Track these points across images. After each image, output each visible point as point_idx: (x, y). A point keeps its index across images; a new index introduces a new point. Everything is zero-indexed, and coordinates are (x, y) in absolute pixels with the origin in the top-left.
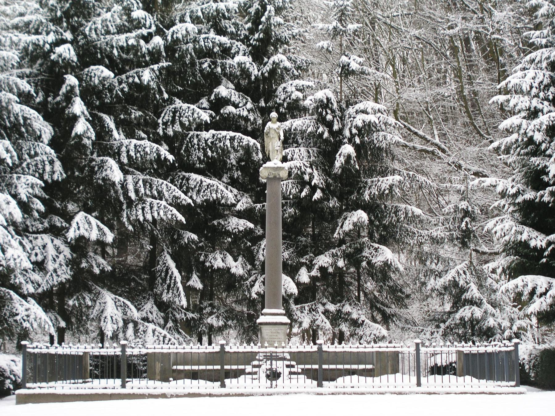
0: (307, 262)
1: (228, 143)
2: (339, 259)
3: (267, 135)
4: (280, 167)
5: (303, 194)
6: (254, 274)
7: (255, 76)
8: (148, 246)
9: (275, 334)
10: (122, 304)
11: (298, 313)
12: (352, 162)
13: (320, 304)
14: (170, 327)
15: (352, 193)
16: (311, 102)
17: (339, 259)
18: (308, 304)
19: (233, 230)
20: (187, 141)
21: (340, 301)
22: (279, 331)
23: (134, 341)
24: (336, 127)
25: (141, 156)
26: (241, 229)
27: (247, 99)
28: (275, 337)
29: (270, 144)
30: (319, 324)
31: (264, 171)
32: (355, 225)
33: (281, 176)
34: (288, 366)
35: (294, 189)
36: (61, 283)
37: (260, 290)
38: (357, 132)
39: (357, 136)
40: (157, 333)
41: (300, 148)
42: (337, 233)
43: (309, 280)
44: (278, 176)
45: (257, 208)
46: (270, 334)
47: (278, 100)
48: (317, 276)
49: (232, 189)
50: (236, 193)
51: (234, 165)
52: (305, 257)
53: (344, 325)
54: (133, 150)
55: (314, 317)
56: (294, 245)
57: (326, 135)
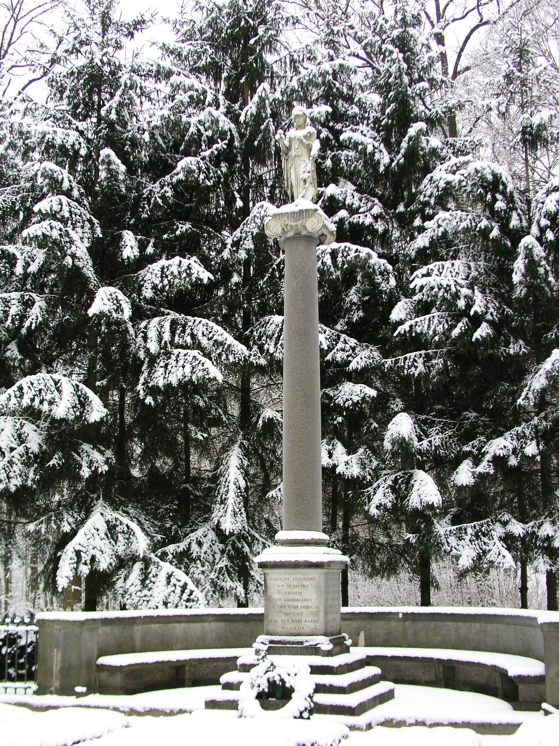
0: (474, 450)
1: (328, 260)
2: (528, 442)
4: (307, 211)
5: (456, 332)
6: (385, 475)
7: (384, 165)
8: (199, 433)
9: (296, 590)
10: (126, 529)
11: (453, 540)
12: (541, 270)
13: (498, 524)
14: (221, 569)
15: (550, 329)
16: (462, 178)
17: (528, 442)
18: (472, 524)
19: (344, 404)
20: (274, 269)
21: (535, 517)
22: (306, 583)
23: (139, 593)
24: (514, 222)
25: (169, 282)
26: (356, 399)
27: (373, 202)
28: (297, 597)
30: (492, 558)
31: (273, 223)
33: (310, 229)
34: (316, 670)
35: (441, 326)
37: (384, 501)
38: (548, 223)
39: (548, 230)
40: (173, 580)
41: (453, 261)
42: (523, 396)
43: (473, 480)
44: (304, 233)
45: (386, 366)
48: (488, 473)
49: (347, 338)
50: (353, 345)
51: (354, 304)
52: (471, 443)
53: (541, 560)
54: (159, 275)
55: (484, 547)
56: (455, 425)
57: (495, 233)
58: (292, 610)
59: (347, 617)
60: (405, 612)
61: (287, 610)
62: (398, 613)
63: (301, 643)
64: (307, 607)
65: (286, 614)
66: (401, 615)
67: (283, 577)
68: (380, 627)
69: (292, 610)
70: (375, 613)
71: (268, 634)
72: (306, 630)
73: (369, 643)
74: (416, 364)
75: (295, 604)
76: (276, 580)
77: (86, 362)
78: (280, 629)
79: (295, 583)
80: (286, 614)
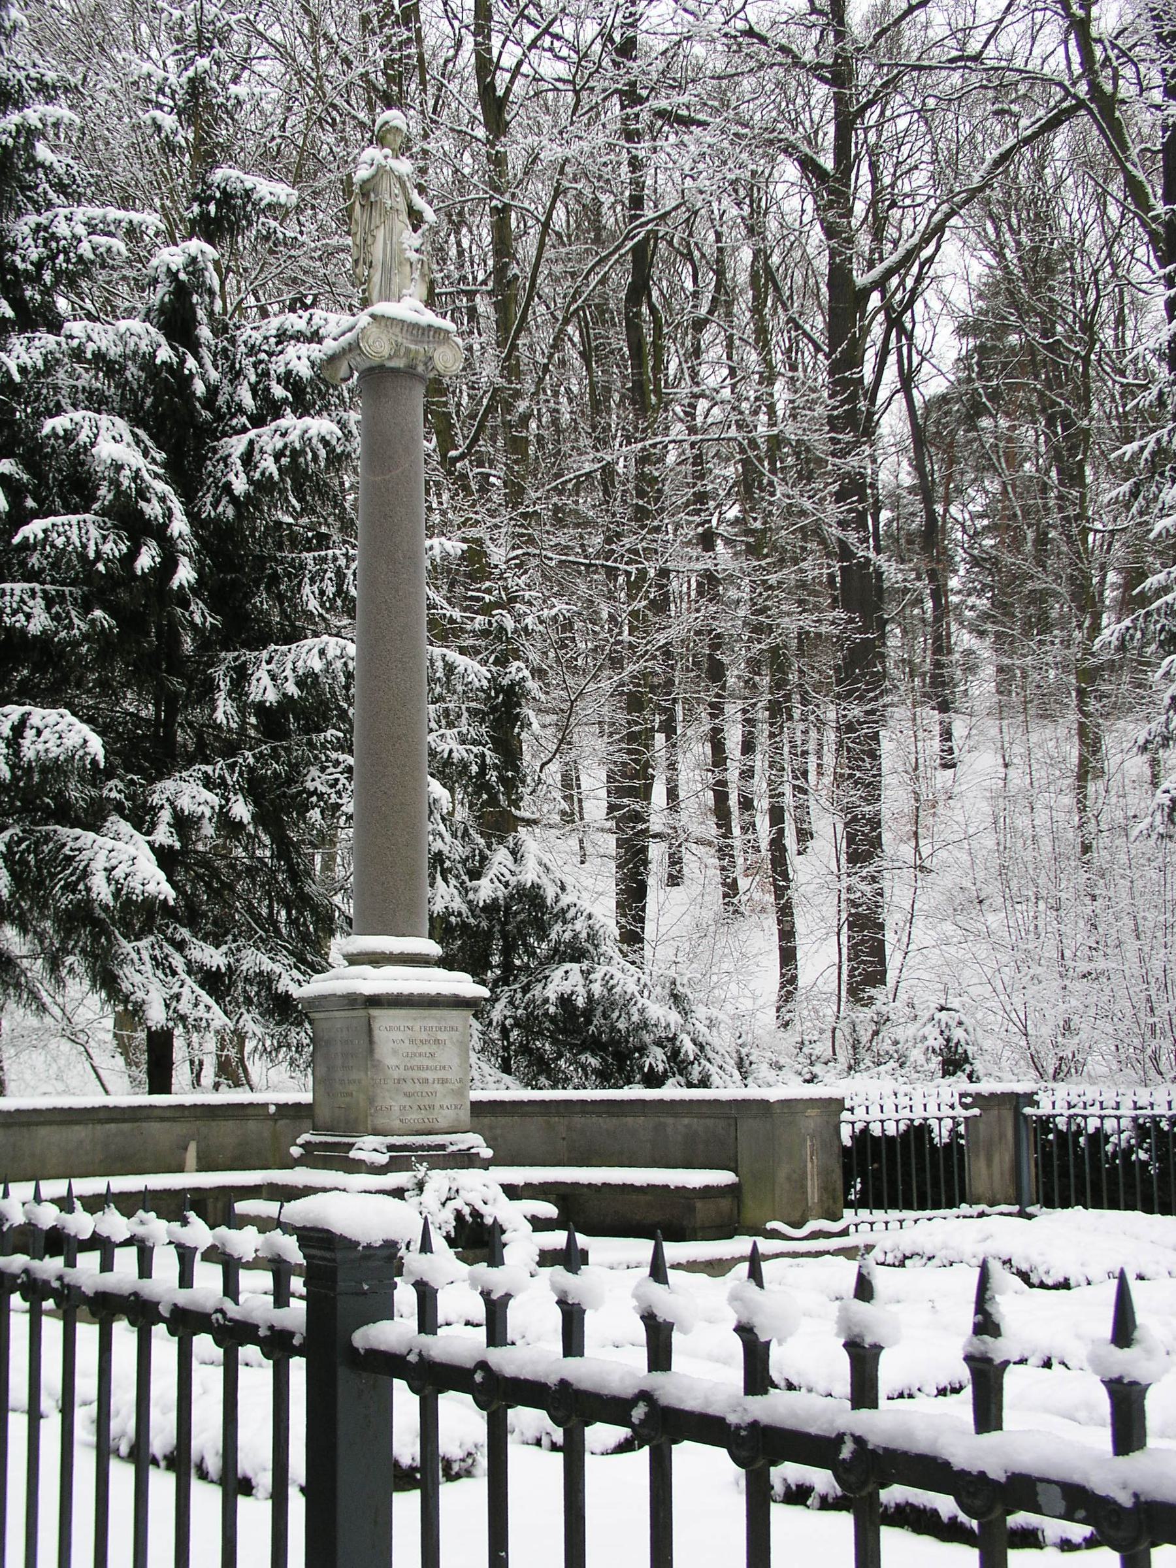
3: (365, 195)
9: (425, 1049)
22: (442, 1036)
28: (426, 1062)
29: (380, 234)
32: (307, 681)
36: (651, 265)
46: (407, 1047)
47: (18, 259)
48: (171, 847)
58: (418, 1087)
59: (168, 1114)
60: (281, 1102)
61: (409, 1087)
62: (266, 1105)
63: (442, 1147)
64: (443, 1081)
65: (407, 1095)
66: (272, 1109)
67: (401, 1024)
68: (226, 1132)
69: (418, 1087)
70: (222, 1105)
71: (376, 1133)
72: (443, 1124)
73: (205, 1165)
74: (26, 609)
75: (424, 1075)
76: (390, 1029)
77: (58, 501)
78: (396, 1124)
79: (424, 1036)
80: (407, 1095)
